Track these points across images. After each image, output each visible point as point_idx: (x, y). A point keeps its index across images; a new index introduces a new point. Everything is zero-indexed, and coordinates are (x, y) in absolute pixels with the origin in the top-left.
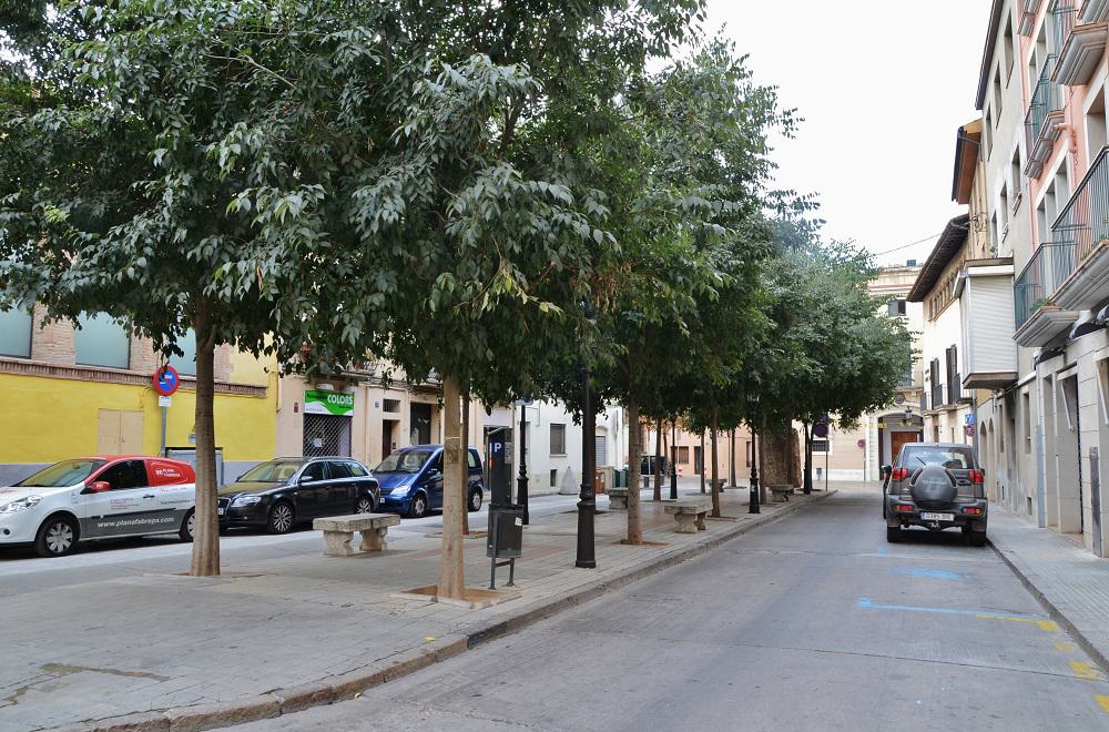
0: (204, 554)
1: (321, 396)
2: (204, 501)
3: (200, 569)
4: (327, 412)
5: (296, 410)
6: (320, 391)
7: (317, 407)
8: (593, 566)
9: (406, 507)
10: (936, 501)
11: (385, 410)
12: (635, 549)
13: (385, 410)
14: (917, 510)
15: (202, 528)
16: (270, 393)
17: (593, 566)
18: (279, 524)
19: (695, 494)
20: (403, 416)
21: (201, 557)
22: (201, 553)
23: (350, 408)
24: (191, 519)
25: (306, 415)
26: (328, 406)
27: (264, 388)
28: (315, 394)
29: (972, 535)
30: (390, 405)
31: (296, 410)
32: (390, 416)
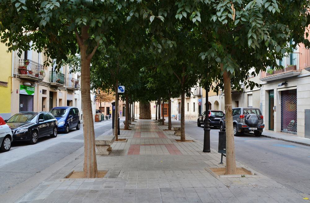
0: (92, 165)
1: (25, 87)
2: (91, 138)
3: (91, 173)
4: (26, 94)
5: (17, 93)
6: (24, 85)
7: (24, 92)
8: (209, 152)
9: (64, 130)
10: (254, 124)
11: (43, 94)
12: (184, 143)
13: (43, 94)
14: (248, 127)
15: (91, 152)
16: (9, 85)
17: (209, 152)
18: (34, 140)
19: (155, 120)
20: (47, 95)
21: (91, 167)
22: (91, 165)
23: (33, 92)
24: (5, 141)
25: (20, 95)
26: (27, 91)
27: (7, 83)
28: (23, 86)
29: (258, 134)
30: (44, 92)
31: (17, 93)
32: (44, 96)
